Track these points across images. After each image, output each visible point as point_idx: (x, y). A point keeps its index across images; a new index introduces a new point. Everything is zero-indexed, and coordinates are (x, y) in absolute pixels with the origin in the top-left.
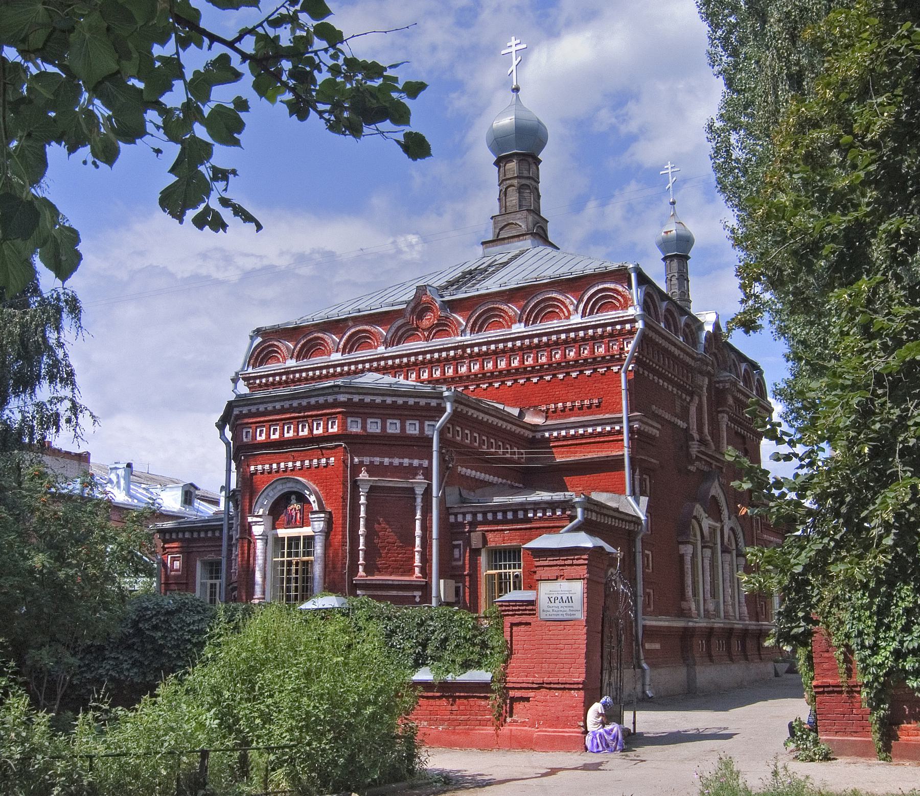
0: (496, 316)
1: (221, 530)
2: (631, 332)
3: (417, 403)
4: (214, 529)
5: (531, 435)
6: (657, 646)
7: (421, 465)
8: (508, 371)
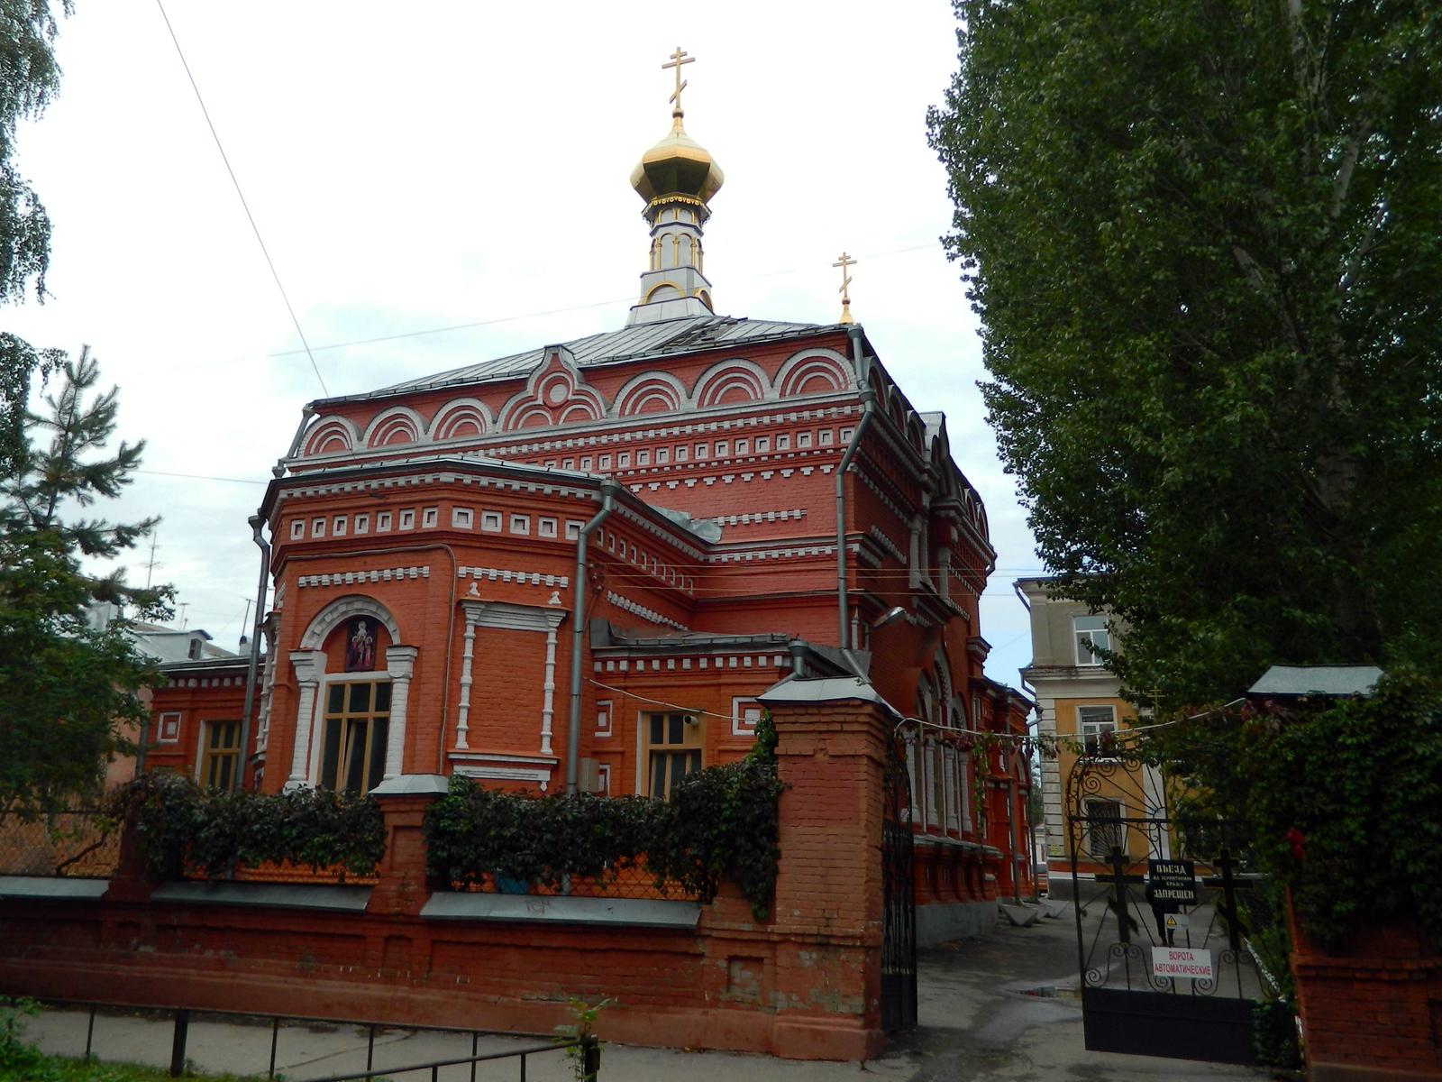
1: (245, 677)
4: (233, 675)
8: (673, 467)
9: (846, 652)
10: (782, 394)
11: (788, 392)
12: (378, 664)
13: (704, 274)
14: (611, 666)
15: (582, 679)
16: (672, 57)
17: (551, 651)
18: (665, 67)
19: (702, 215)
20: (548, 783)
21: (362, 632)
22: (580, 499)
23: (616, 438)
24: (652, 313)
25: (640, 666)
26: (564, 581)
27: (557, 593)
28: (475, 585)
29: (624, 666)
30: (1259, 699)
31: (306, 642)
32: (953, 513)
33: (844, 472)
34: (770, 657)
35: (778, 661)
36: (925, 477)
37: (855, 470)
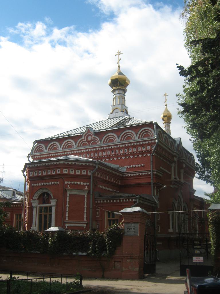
0: (40, 148)
2: (155, 143)
3: (78, 164)
5: (122, 175)
6: (161, 243)
7: (87, 185)
9: (153, 196)
10: (139, 138)
11: (140, 137)
12: (49, 202)
13: (126, 106)
14: (99, 202)
15: (92, 205)
16: (117, 53)
17: (86, 199)
18: (116, 55)
19: (125, 91)
20: (86, 227)
21: (46, 196)
22: (91, 166)
23: (102, 148)
24: (114, 115)
25: (105, 201)
26: (88, 184)
27: (87, 186)
28: (69, 185)
29: (102, 201)
30: (210, 210)
31: (34, 198)
32: (184, 161)
33: (152, 156)
34: (132, 199)
35: (134, 200)
36: (175, 154)
37: (155, 155)
